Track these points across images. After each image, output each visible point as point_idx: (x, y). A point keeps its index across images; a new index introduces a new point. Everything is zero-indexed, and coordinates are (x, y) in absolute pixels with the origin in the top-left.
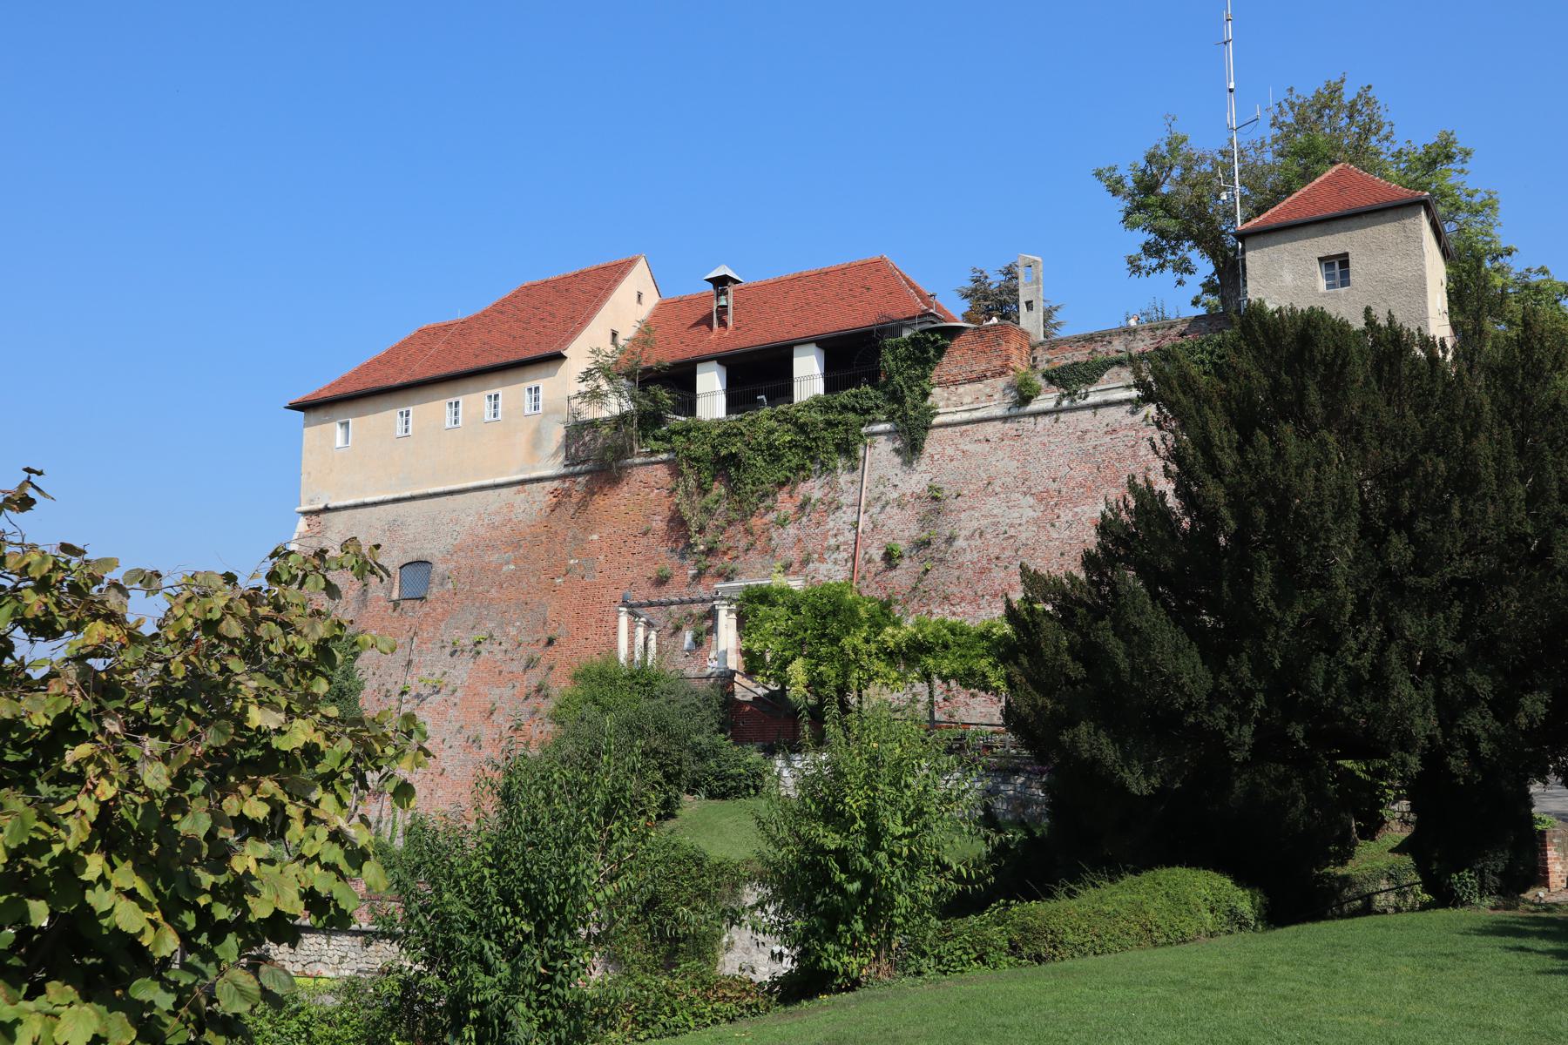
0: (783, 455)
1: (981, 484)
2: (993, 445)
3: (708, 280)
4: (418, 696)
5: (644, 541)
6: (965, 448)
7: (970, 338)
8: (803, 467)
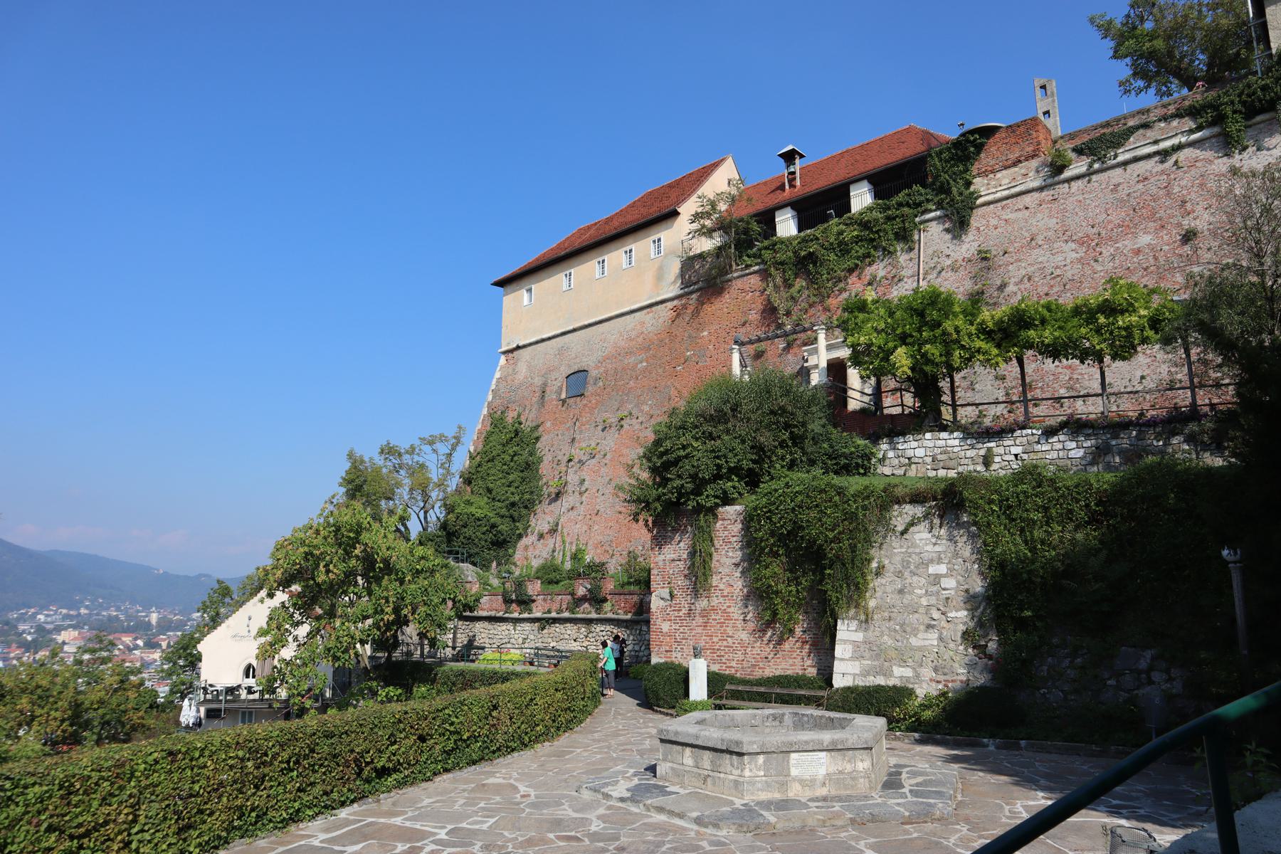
4: (580, 461)
6: (1007, 217)
8: (868, 255)
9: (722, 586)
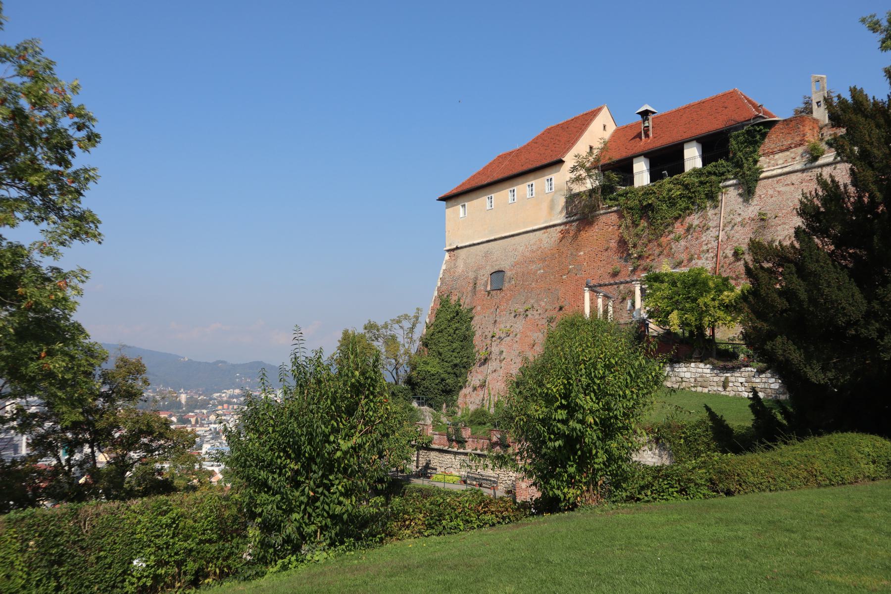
0: (677, 202)
1: (789, 209)
2: (796, 186)
3: (638, 113)
4: (500, 338)
5: (606, 254)
6: (780, 190)
7: (781, 127)
8: (688, 208)
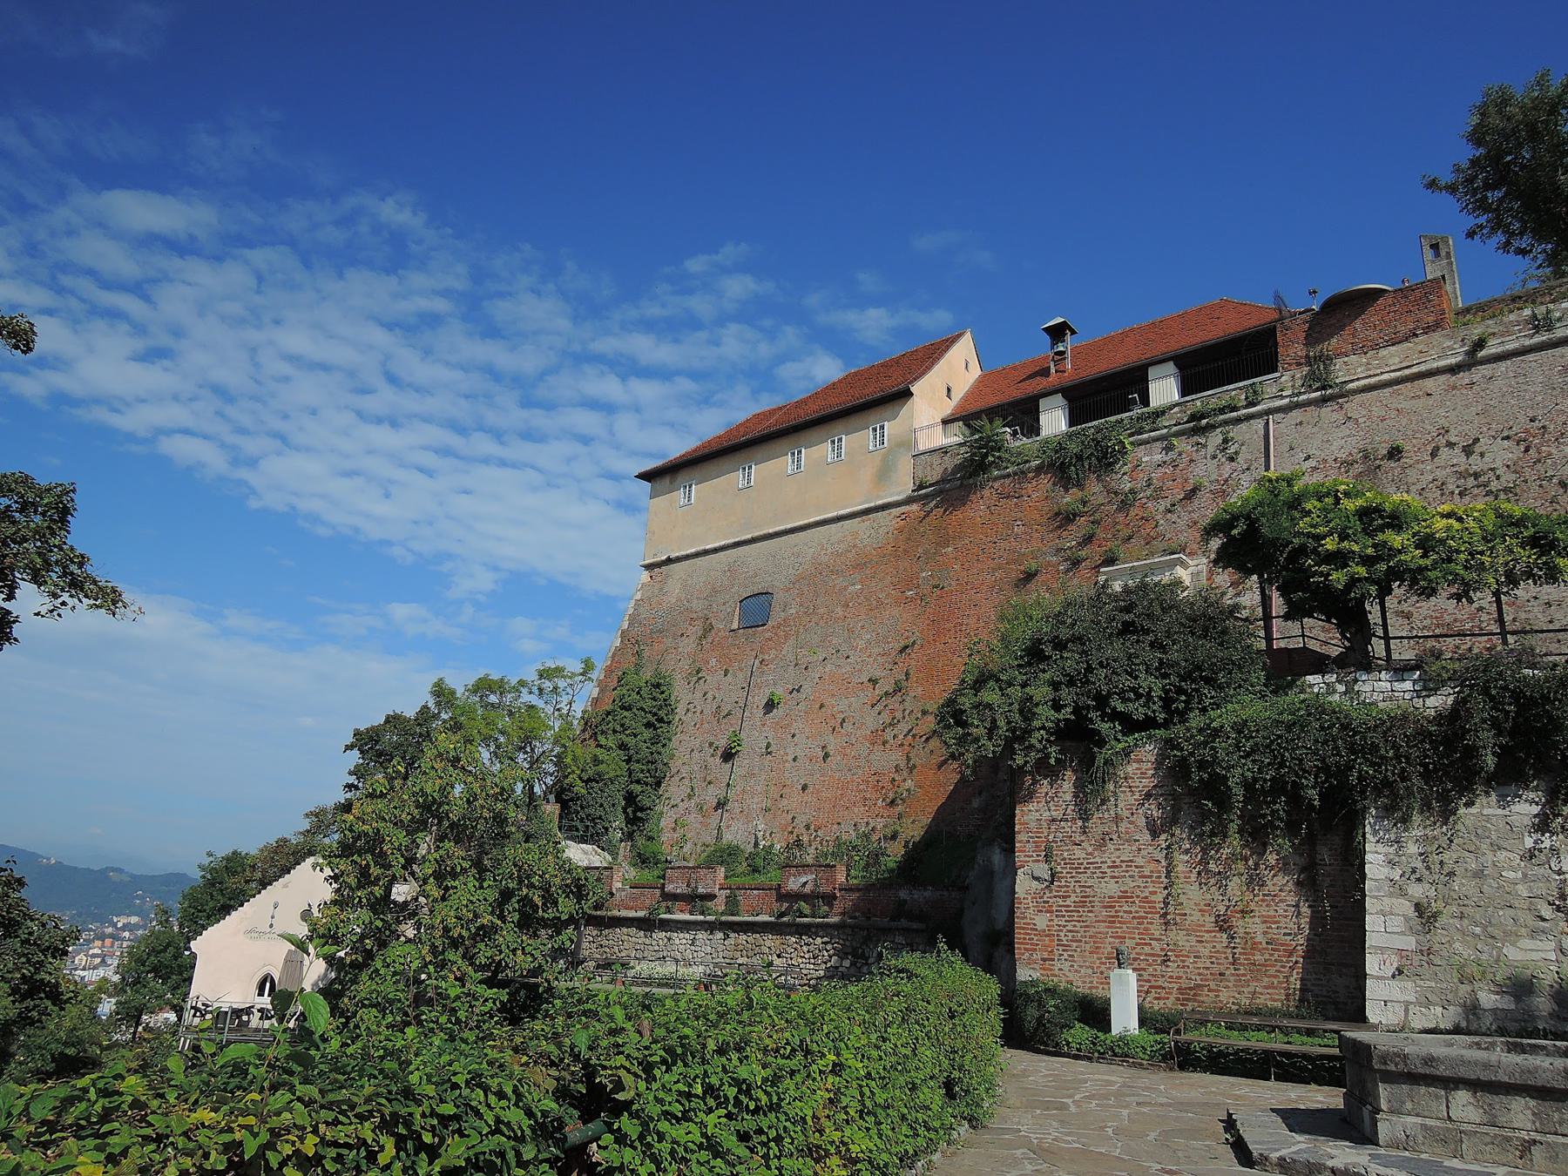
3: (1046, 330)
9: (1140, 861)
